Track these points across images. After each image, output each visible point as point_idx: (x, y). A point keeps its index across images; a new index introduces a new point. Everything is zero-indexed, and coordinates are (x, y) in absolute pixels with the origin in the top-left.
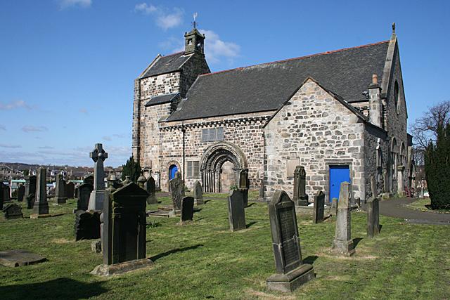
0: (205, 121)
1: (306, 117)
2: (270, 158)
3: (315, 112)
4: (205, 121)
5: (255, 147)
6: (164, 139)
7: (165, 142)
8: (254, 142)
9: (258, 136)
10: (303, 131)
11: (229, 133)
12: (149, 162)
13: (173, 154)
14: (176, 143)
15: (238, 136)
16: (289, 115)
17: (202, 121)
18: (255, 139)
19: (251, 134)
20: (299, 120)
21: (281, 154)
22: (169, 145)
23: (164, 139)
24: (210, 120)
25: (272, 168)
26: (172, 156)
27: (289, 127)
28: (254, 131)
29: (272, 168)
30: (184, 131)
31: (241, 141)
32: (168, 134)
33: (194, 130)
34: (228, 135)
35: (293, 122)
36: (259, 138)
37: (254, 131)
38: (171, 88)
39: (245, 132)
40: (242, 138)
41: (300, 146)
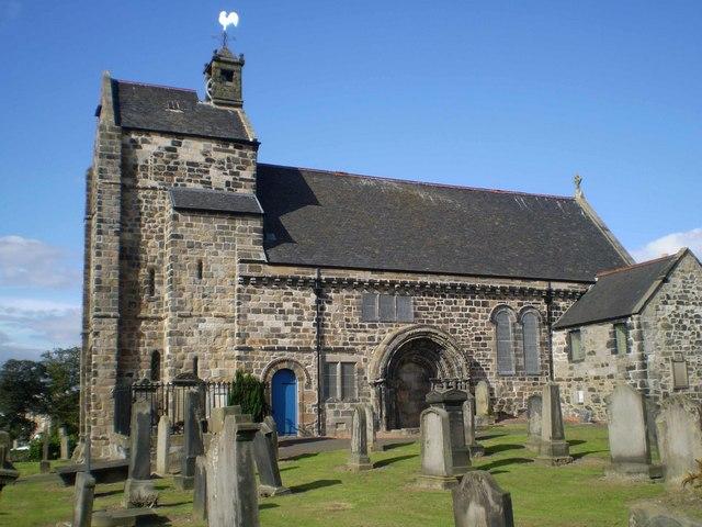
0: (378, 278)
1: (688, 304)
2: (651, 358)
3: (697, 299)
4: (378, 278)
5: (477, 339)
6: (252, 304)
7: (256, 311)
8: (474, 330)
9: (480, 321)
10: (686, 322)
11: (427, 309)
12: (188, 360)
13: (283, 342)
14: (293, 318)
15: (443, 315)
16: (669, 297)
17: (367, 276)
18: (476, 324)
19: (468, 316)
20: (681, 307)
21: (663, 354)
22: (270, 322)
23: (252, 304)
24: (387, 277)
25: (654, 375)
26: (280, 349)
27: (670, 316)
28: (474, 310)
29: (654, 375)
30: (319, 293)
31: (451, 326)
32: (267, 295)
33: (344, 293)
34: (423, 313)
35: (674, 309)
36: (483, 324)
37: (474, 310)
38: (230, 178)
39: (457, 309)
40: (452, 321)
41: (685, 344)
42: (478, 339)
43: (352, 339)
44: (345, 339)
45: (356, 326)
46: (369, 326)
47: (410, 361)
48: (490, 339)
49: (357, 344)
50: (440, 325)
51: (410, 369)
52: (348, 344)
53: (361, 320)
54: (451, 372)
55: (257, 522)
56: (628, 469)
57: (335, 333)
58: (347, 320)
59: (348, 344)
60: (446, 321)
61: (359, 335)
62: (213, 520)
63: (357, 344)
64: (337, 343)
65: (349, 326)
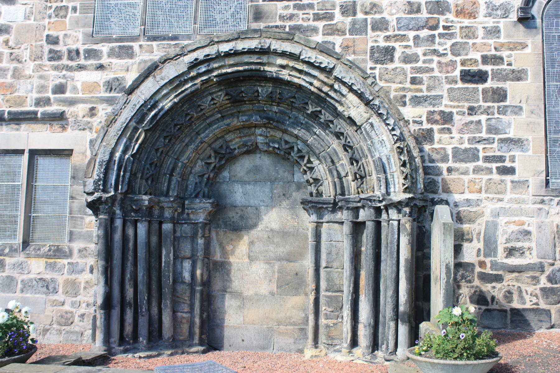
8: (456, 50)
18: (469, 32)
42: (474, 77)
43: (60, 89)
44: (42, 88)
45: (74, 54)
46: (112, 53)
47: (252, 150)
48: (518, 76)
49: (72, 102)
50: (338, 41)
51: (256, 169)
52: (47, 102)
53: (91, 37)
54: (360, 177)
55: (105, 313)
56: (98, 316)
57: (17, 75)
58: (53, 40)
59: (47, 102)
60: (358, 29)
61: (81, 77)
62: (29, 309)
63: (72, 102)
64: (21, 101)
65: (55, 56)
